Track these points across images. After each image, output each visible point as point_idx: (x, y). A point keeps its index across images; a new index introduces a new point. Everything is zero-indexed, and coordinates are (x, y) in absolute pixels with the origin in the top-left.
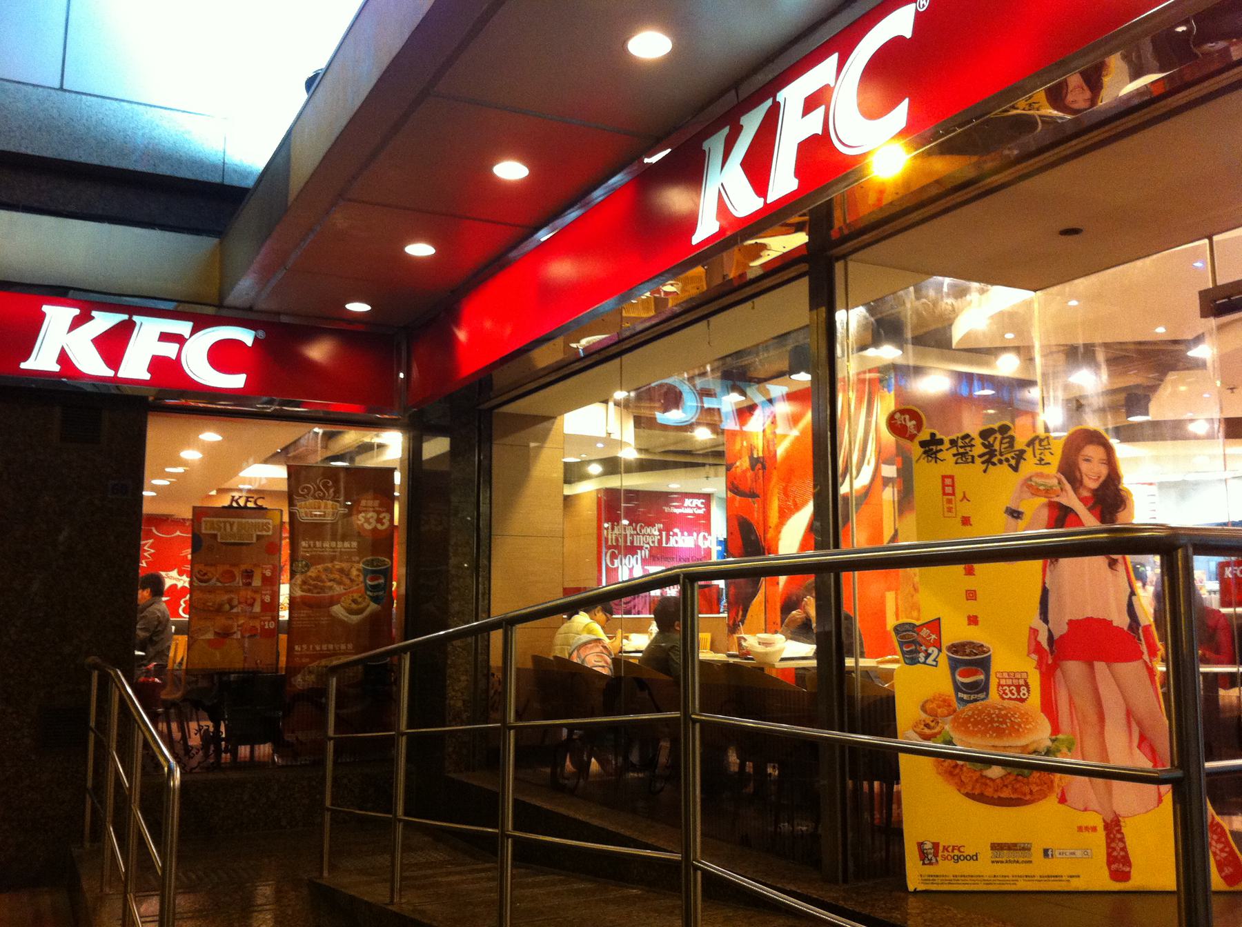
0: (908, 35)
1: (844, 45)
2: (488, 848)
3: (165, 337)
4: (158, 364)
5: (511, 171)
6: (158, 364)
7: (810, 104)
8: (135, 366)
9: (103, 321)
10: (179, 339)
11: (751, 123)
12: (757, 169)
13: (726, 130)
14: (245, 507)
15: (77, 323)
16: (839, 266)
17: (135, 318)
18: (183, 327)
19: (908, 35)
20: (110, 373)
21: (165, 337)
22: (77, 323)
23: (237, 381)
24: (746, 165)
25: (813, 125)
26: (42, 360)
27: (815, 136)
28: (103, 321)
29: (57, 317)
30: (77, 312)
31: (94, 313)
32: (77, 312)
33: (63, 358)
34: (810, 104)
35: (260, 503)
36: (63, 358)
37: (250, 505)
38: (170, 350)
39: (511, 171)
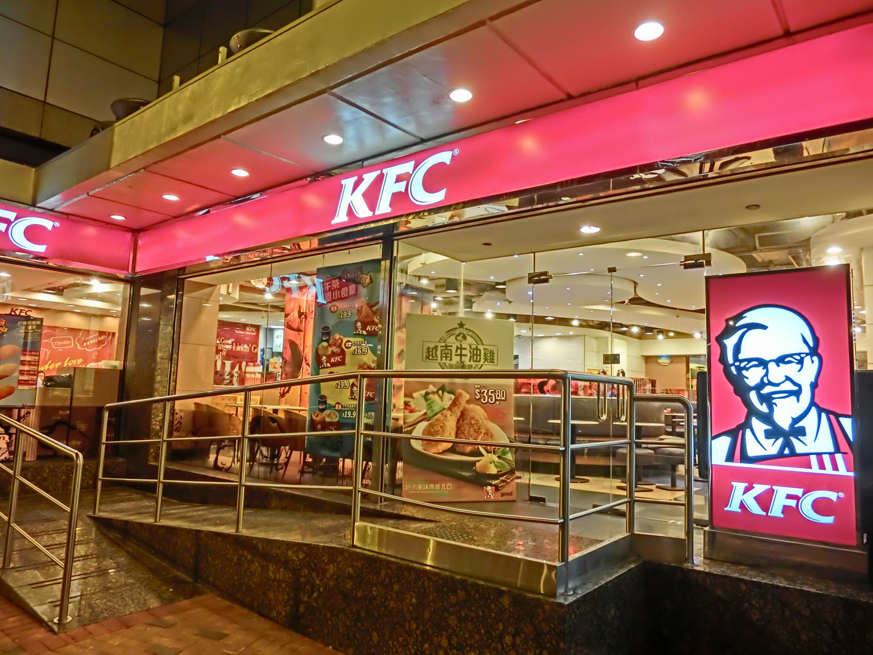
0: (448, 163)
1: (418, 159)
2: (151, 489)
3: (789, 497)
4: (786, 509)
5: (240, 173)
6: (786, 509)
7: (399, 179)
8: (776, 511)
9: (759, 489)
10: (797, 498)
11: (369, 178)
12: (371, 197)
13: (355, 178)
14: (19, 315)
15: (746, 490)
16: (395, 242)
17: (774, 487)
18: (798, 492)
19: (448, 163)
20: (764, 514)
21: (789, 497)
22: (746, 490)
23: (830, 520)
24: (365, 195)
25: (401, 187)
26: (734, 506)
27: (400, 192)
28: (759, 489)
29: (739, 487)
30: (746, 484)
31: (754, 485)
32: (746, 484)
33: (742, 505)
34: (399, 179)
35: (29, 313)
36: (742, 505)
37: (22, 314)
38: (792, 503)
39: (240, 173)
